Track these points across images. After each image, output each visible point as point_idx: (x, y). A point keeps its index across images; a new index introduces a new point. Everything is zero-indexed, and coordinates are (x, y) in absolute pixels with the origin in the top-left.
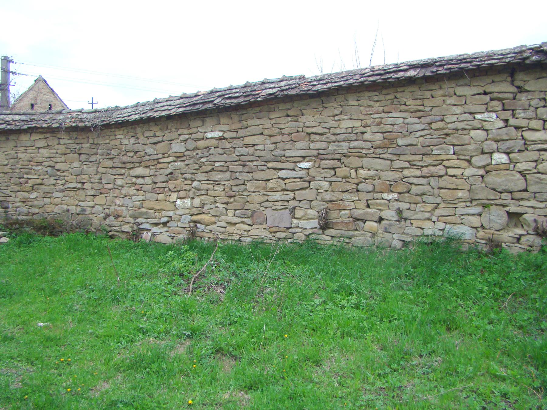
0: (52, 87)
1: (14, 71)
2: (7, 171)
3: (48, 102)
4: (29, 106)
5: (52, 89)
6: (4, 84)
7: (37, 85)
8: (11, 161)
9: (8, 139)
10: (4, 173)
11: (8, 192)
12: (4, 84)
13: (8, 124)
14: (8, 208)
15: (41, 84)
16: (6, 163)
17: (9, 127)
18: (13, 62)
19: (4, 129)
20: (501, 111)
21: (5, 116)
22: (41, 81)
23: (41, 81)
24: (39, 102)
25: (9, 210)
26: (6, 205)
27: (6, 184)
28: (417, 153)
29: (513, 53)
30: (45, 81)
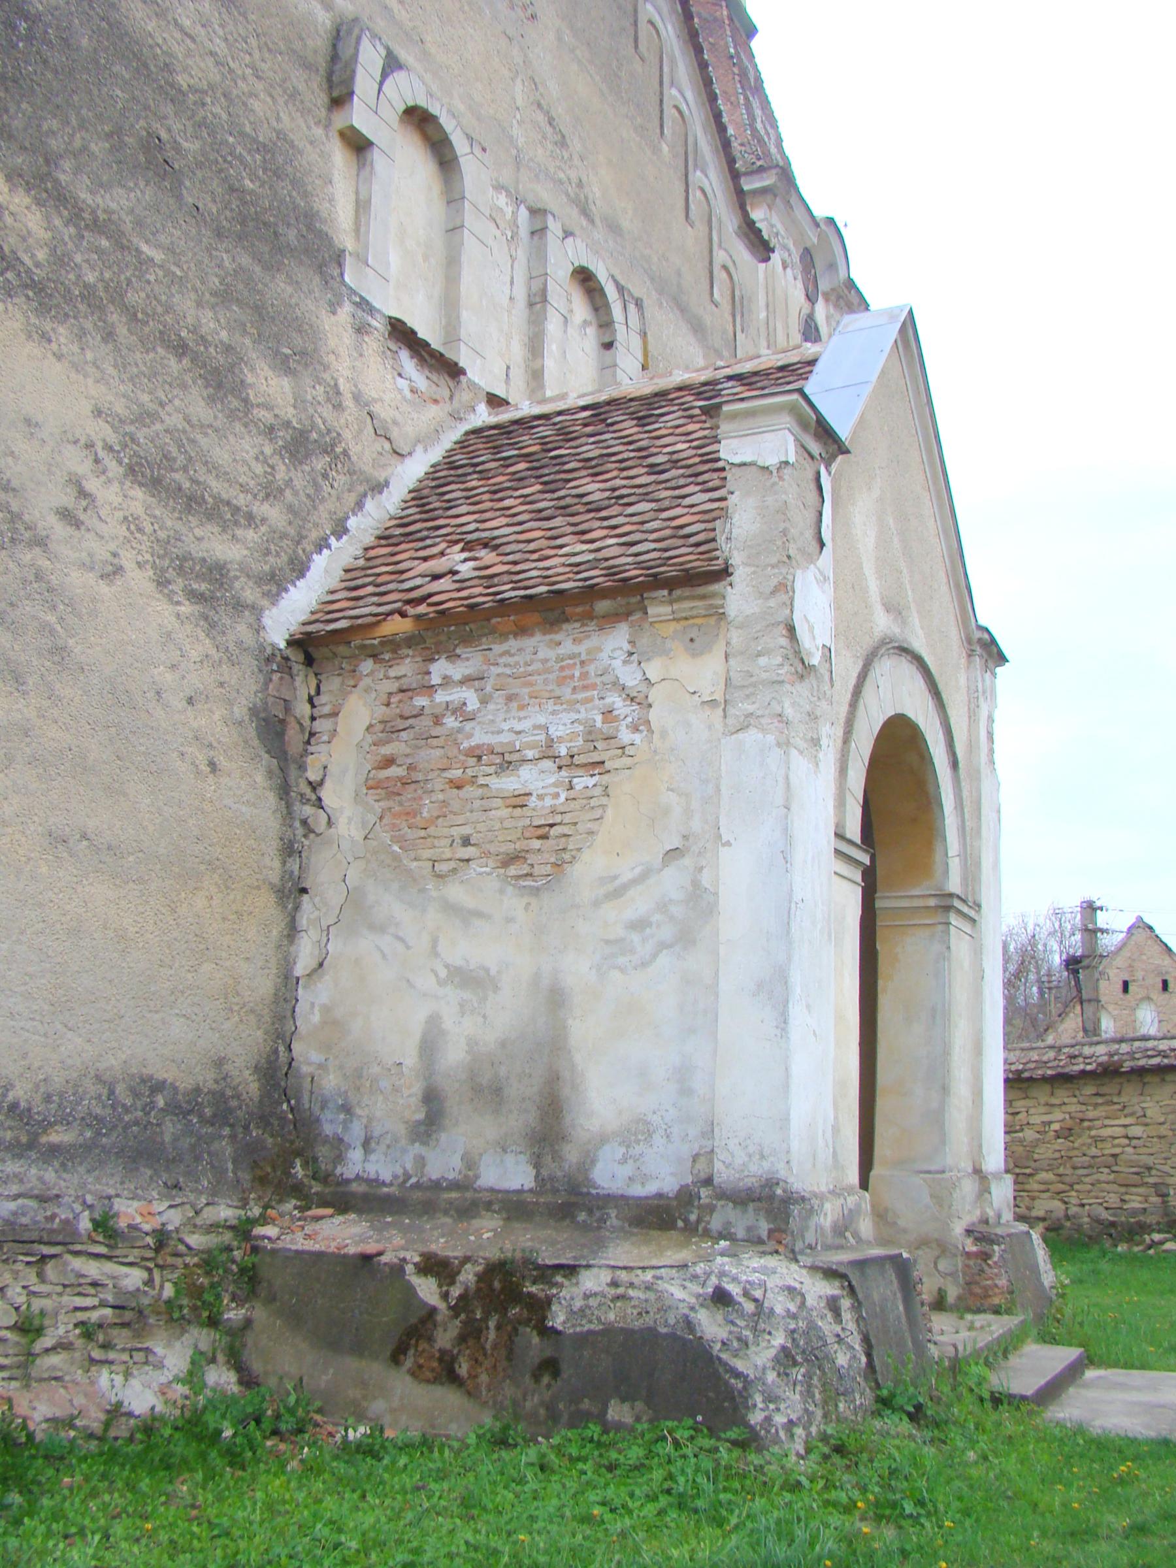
0: (1164, 940)
1: (1105, 927)
2: (1165, 1133)
3: (1160, 973)
4: (1120, 986)
5: (1166, 945)
6: (1088, 957)
7: (1134, 938)
8: (1171, 1117)
9: (1163, 1080)
10: (1160, 1137)
11: (1166, 1168)
12: (1088, 957)
13: (1164, 1057)
14: (1167, 1195)
15: (1140, 935)
16: (1162, 1120)
17: (1166, 1061)
18: (1101, 909)
19: (1159, 1065)
20: (579, 1266)
21: (1156, 1043)
22: (1141, 927)
23: (1141, 927)
24: (1139, 975)
25: (1169, 1199)
26: (1165, 1191)
27: (1163, 1155)
28: (46, 1239)
29: (1139, 1166)
30: (1150, 928)
